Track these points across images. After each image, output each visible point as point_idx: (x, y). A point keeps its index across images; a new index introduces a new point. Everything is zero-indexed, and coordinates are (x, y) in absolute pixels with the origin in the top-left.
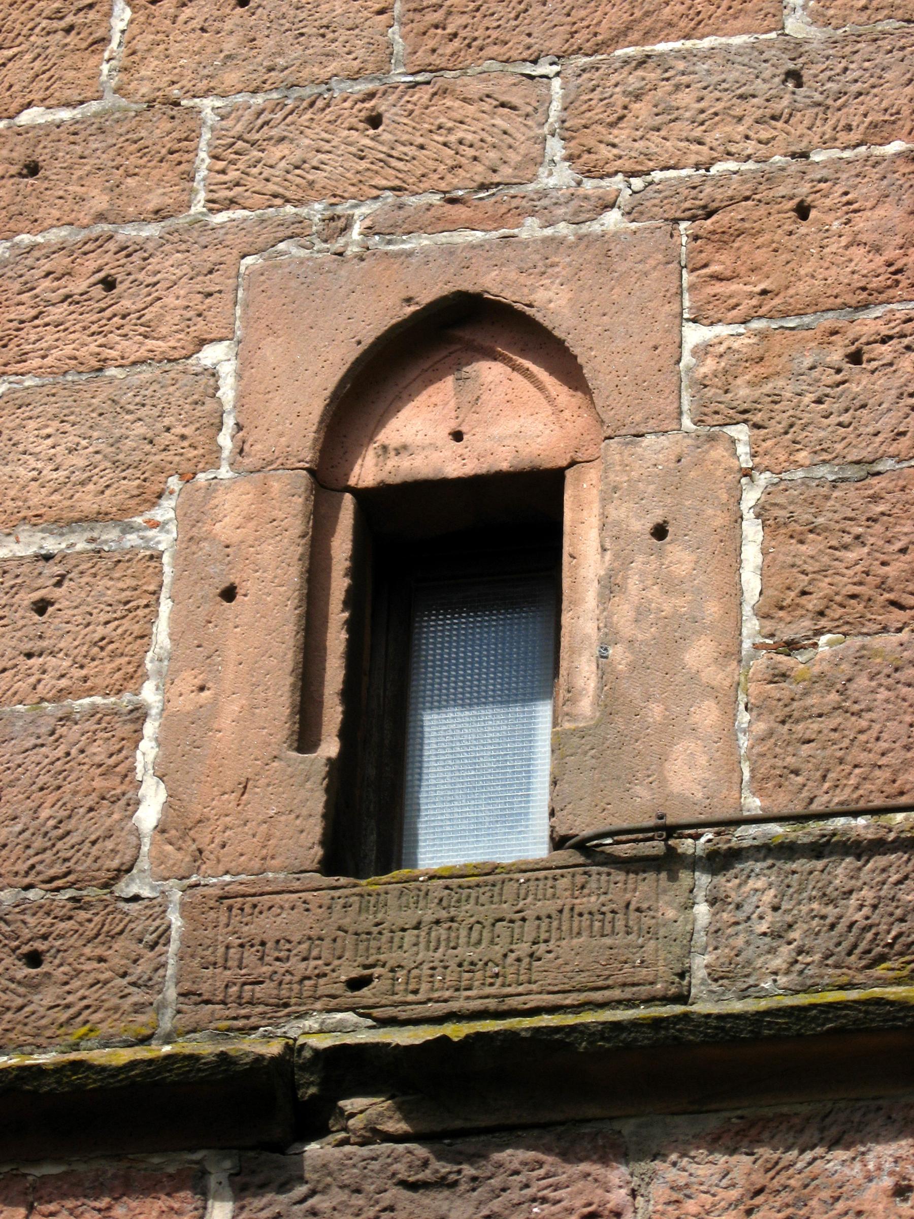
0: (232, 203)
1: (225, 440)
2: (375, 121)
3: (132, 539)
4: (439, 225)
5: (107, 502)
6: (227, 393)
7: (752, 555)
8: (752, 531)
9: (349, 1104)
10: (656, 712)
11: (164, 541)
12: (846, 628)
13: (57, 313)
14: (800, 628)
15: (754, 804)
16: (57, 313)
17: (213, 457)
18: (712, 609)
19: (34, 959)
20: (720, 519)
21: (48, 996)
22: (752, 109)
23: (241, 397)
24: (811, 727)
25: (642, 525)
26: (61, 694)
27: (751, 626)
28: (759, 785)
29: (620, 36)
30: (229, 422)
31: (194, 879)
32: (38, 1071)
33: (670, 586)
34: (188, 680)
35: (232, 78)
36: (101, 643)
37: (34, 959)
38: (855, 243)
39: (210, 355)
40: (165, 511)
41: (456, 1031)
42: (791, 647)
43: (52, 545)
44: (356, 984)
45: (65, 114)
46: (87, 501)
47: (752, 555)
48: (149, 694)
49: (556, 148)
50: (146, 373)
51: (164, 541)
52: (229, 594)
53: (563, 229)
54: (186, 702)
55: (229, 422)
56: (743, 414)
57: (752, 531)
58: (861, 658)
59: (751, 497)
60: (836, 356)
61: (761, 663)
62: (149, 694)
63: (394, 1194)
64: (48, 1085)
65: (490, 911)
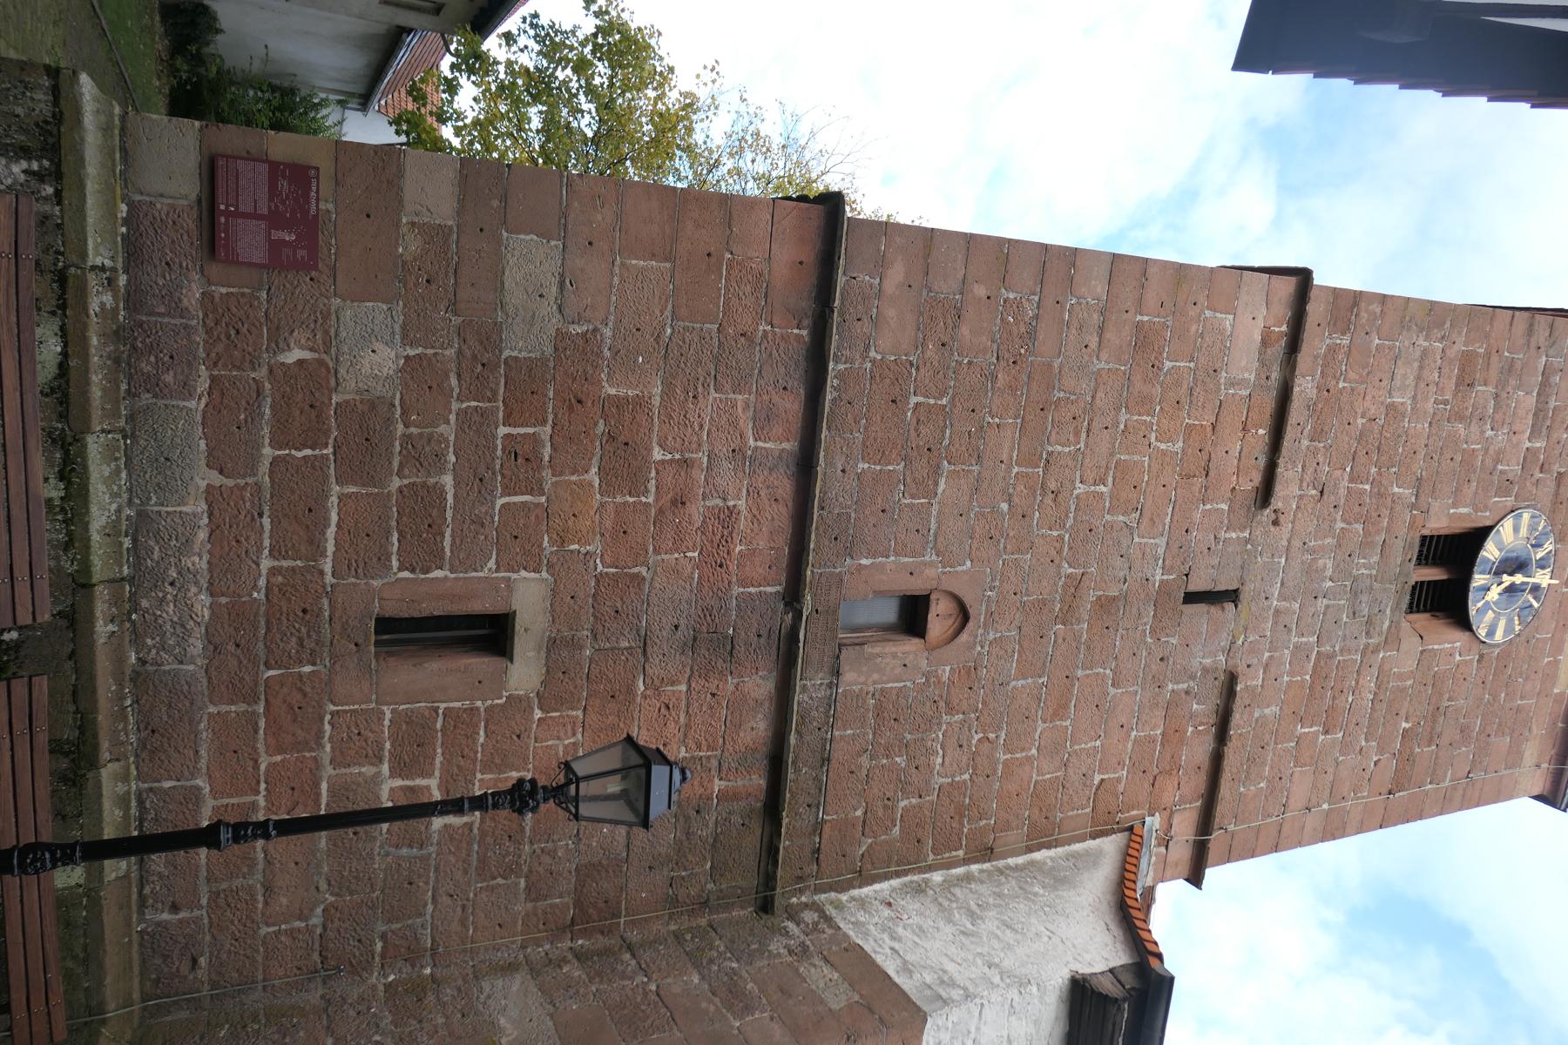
0: (1004, 564)
1: (948, 569)
2: (1015, 594)
3: (929, 550)
4: (987, 610)
5: (939, 544)
6: (959, 568)
7: (896, 685)
8: (902, 684)
9: (790, 615)
10: (864, 669)
11: (927, 558)
12: (875, 706)
13: (987, 527)
14: (877, 696)
15: (840, 691)
16: (987, 527)
17: (944, 567)
18: (885, 678)
19: (836, 539)
20: (904, 678)
21: (827, 543)
22: (996, 676)
23: (957, 572)
24: (855, 701)
25: (907, 662)
26: (896, 538)
27: (880, 686)
28: (845, 691)
29: (1021, 646)
30: (952, 570)
31: (709, 994)
32: (808, 556)
33: (892, 669)
34: (893, 566)
35: (1034, 561)
36: (906, 546)
37: (836, 539)
38: (960, 700)
39: (968, 563)
40: (934, 557)
41: (801, 645)
42: (873, 695)
43: (932, 531)
44: (817, 611)
45: (1035, 523)
46: (941, 539)
47: (896, 685)
48: (892, 558)
49: (999, 635)
50: (967, 548)
51: (927, 558)
52: (911, 574)
53: (979, 638)
54: (888, 567)
55: (952, 570)
56: (927, 680)
57: (902, 684)
58: (868, 710)
59: (908, 684)
60: (936, 698)
61: (871, 689)
62: (892, 558)
63: (768, 626)
64: (804, 557)
65: (827, 639)
